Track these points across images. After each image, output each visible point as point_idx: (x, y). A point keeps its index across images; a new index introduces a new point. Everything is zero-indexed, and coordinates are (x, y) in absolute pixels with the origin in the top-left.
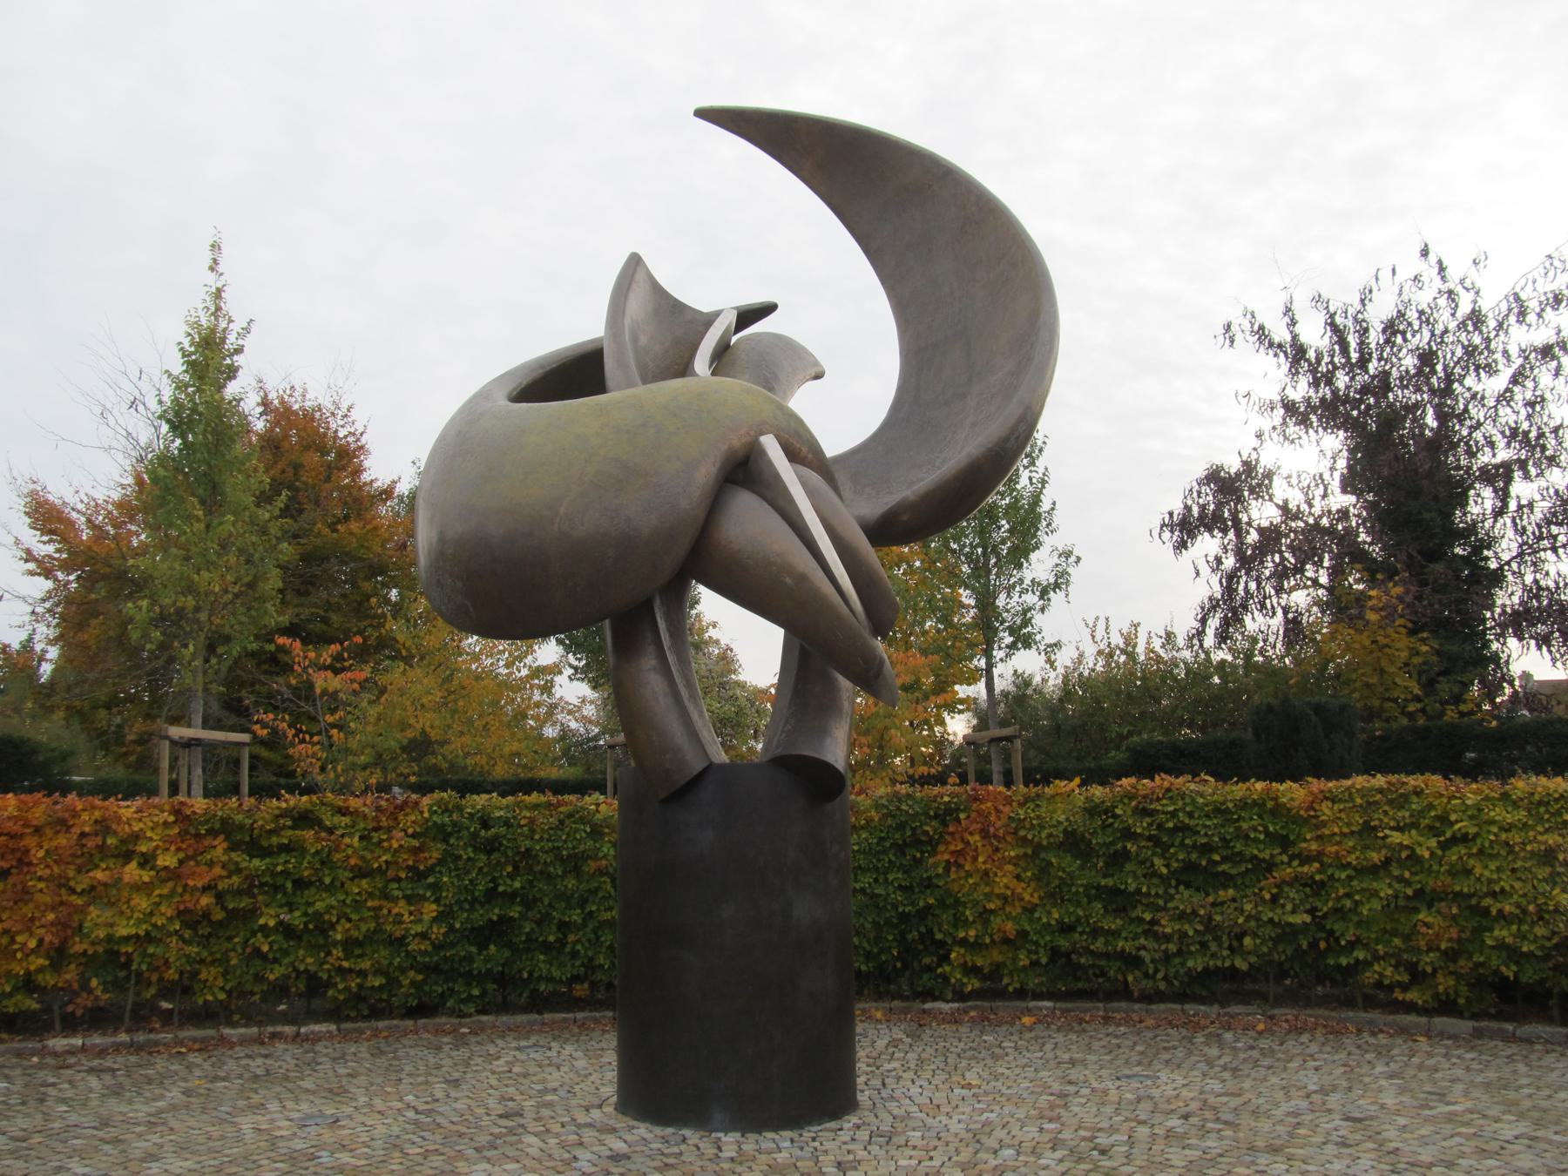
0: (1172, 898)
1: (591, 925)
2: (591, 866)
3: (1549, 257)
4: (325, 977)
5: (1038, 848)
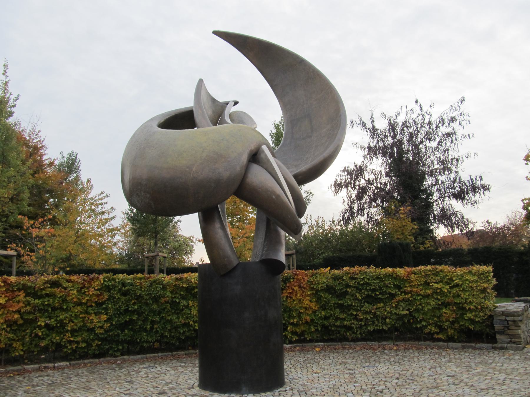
0: (363, 307)
1: (162, 322)
3: (452, 106)
4: (63, 344)
5: (317, 291)
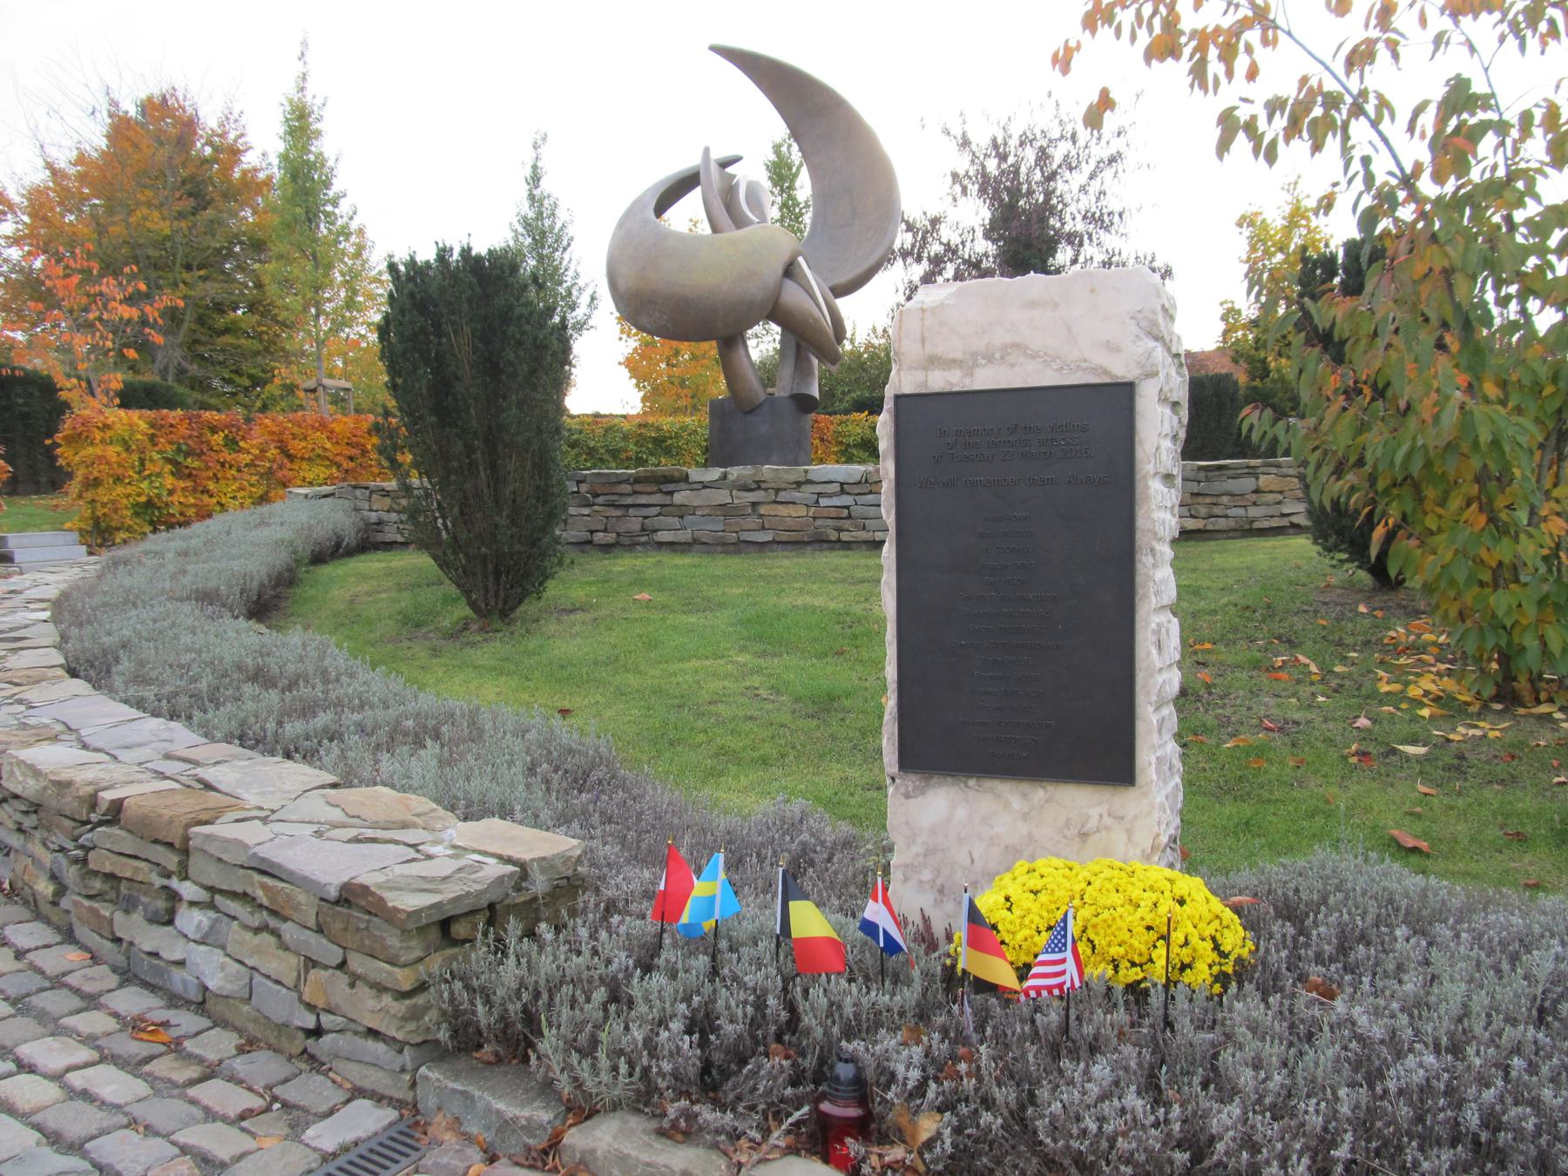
2: (623, 456)
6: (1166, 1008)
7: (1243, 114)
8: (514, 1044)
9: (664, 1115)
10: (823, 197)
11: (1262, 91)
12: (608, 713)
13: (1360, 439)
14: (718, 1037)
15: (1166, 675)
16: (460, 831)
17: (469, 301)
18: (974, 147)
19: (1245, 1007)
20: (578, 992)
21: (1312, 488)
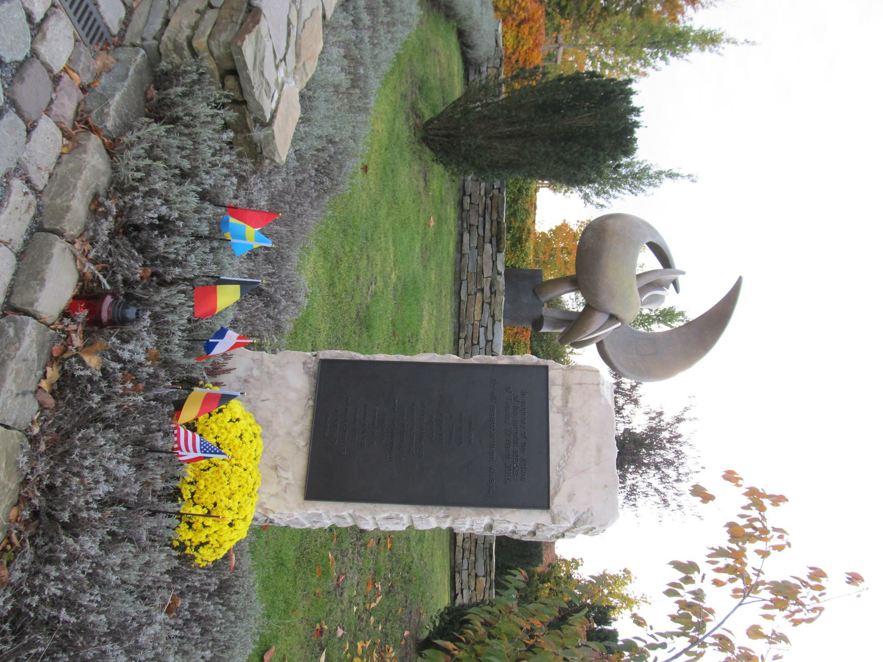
2: (512, 219)
6: (164, 512)
7: (696, 576)
8: (158, 110)
9: (108, 198)
10: (654, 338)
11: (707, 587)
12: (364, 195)
13: (504, 635)
14: (157, 236)
15: (371, 521)
16: (293, 89)
17: (608, 125)
18: (677, 425)
19: (162, 561)
20: (188, 152)
21: (477, 608)
